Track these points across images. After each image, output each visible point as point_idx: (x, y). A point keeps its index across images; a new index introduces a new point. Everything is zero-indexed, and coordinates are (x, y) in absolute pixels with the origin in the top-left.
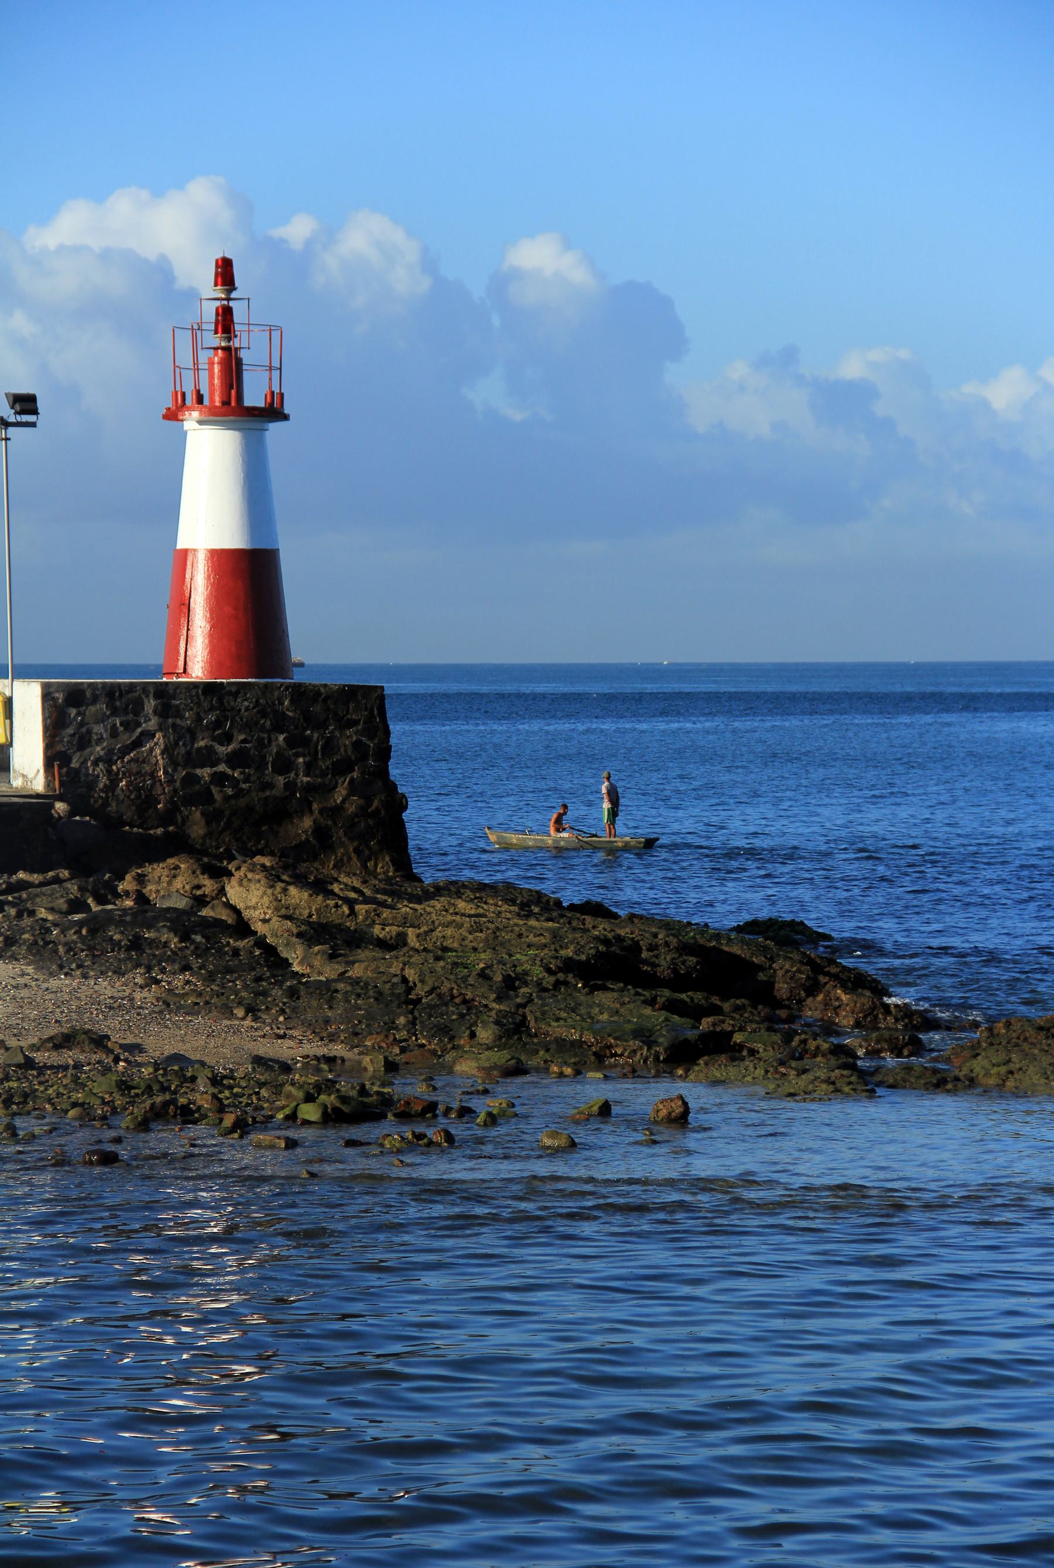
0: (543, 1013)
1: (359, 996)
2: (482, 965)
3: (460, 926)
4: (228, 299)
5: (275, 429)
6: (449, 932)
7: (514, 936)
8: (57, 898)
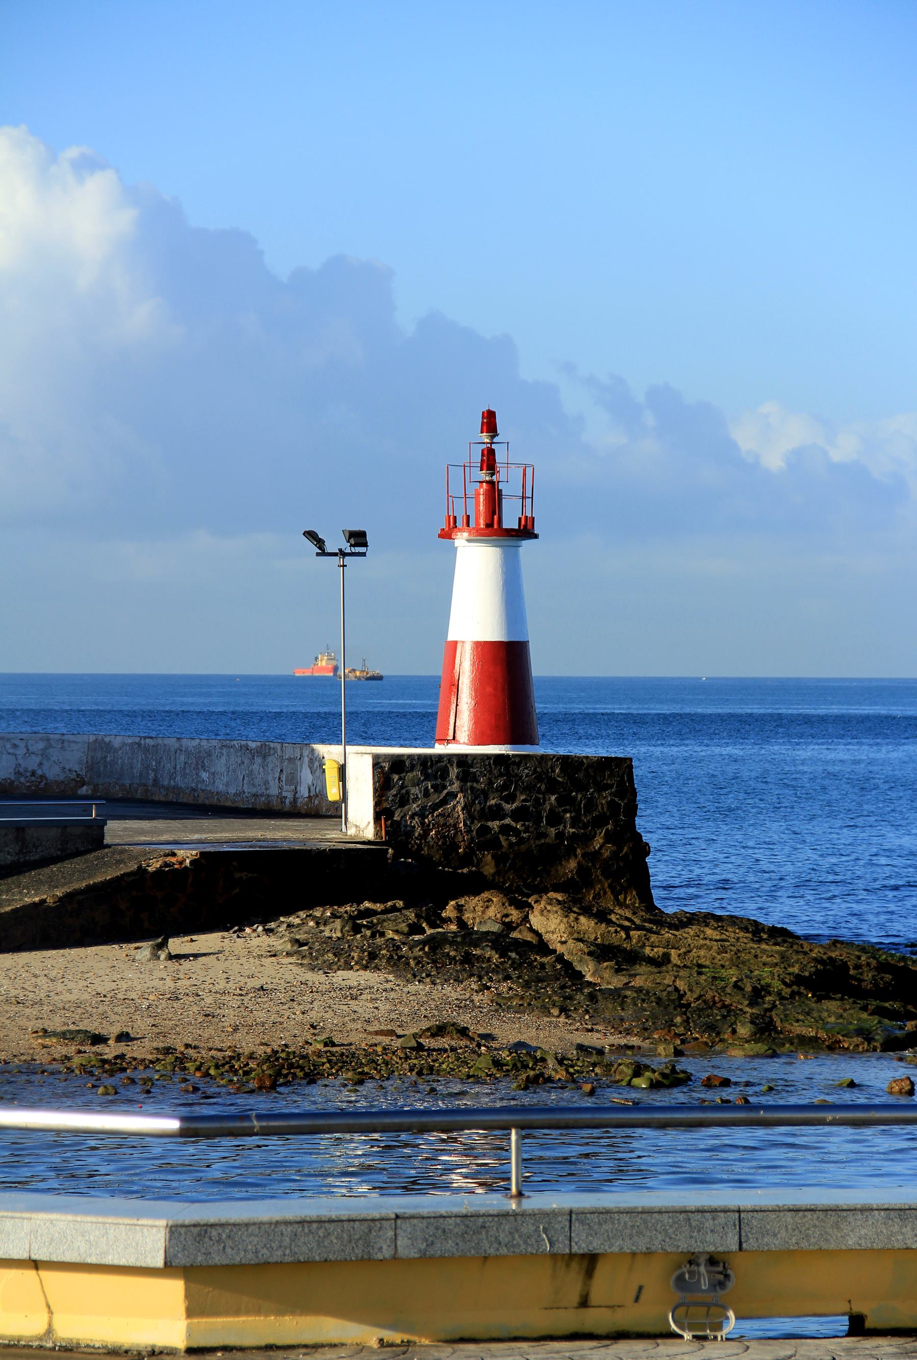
0: (786, 1016)
1: (643, 1001)
2: (734, 979)
3: (710, 949)
4: (491, 443)
5: (526, 545)
6: (702, 953)
7: (751, 956)
8: (400, 923)
